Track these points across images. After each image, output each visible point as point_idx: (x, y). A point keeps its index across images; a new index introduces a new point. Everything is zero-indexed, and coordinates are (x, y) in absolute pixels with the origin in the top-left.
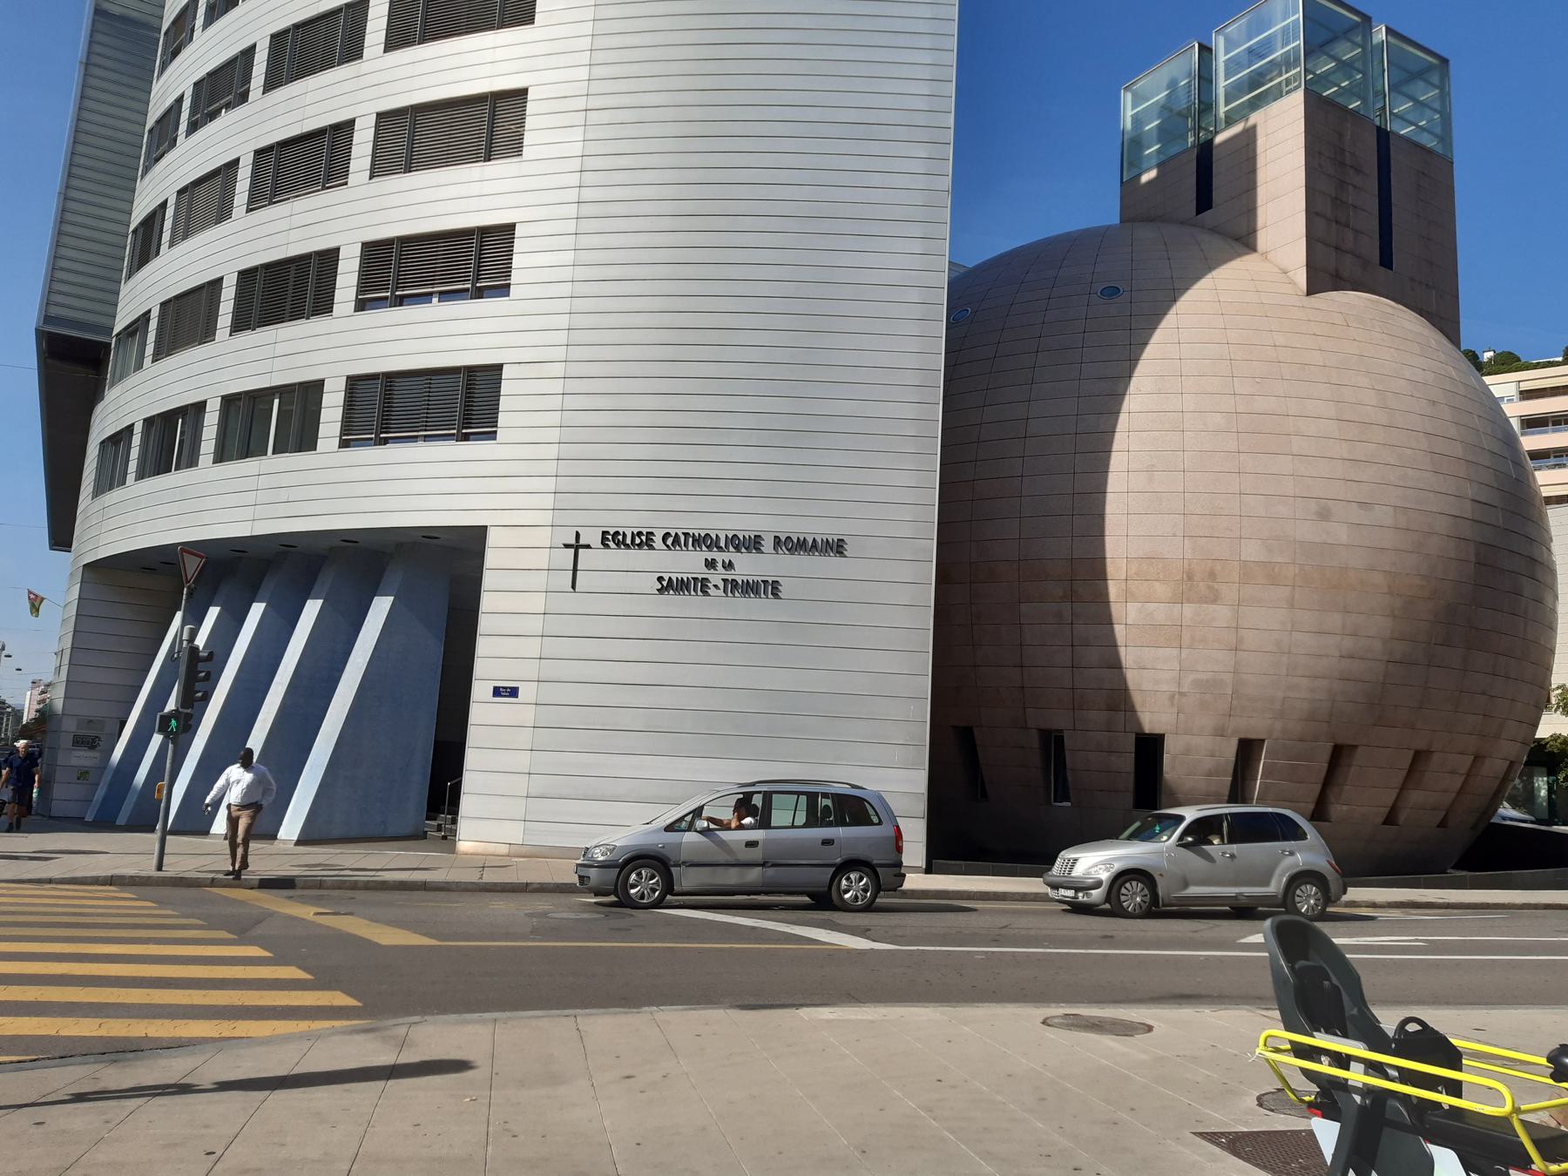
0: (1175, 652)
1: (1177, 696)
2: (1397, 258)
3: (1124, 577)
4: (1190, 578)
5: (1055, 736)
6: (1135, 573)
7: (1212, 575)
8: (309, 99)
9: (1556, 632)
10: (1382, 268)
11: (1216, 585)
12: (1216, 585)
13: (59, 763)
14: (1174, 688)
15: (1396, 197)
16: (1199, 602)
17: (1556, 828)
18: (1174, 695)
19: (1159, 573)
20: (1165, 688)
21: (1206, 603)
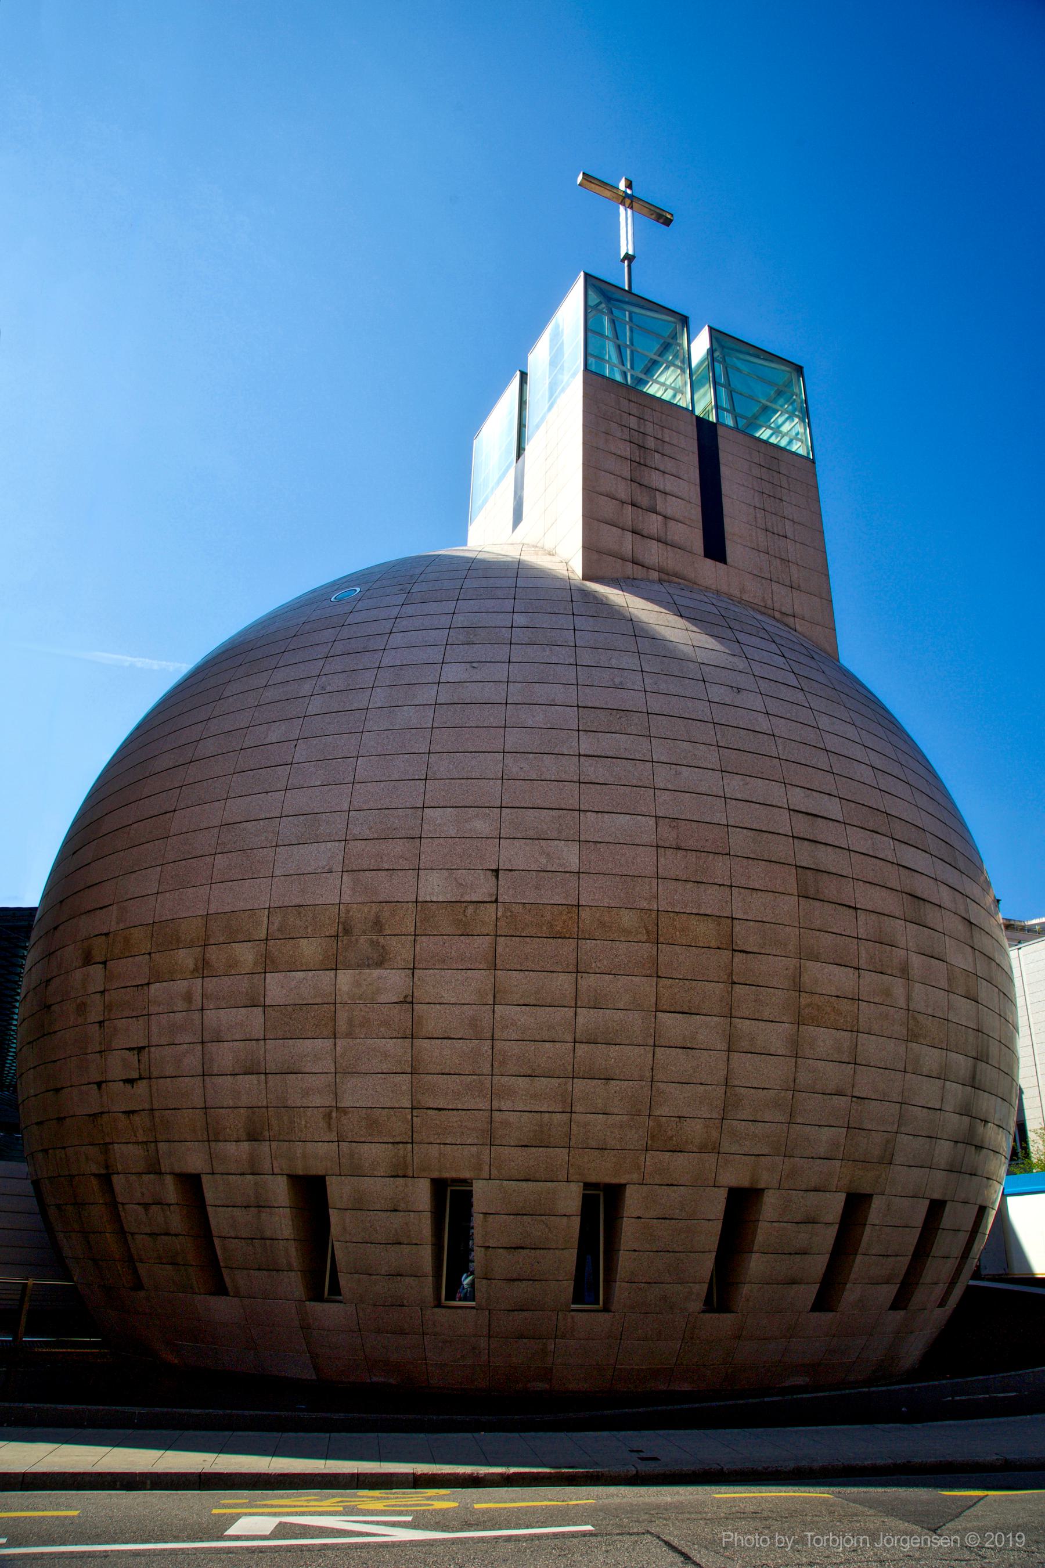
0: (328, 1043)
1: (334, 1115)
2: (732, 549)
3: (263, 936)
4: (347, 931)
5: (451, 1190)
6: (278, 930)
7: (378, 925)
8: (270, 695)
9: (1015, 1006)
10: (708, 560)
11: (381, 940)
12: (381, 940)
13: (289, 1209)
14: (328, 1101)
15: (728, 487)
16: (360, 966)
17: (976, 1397)
18: (331, 1112)
19: (307, 927)
20: (317, 1101)
21: (369, 966)
